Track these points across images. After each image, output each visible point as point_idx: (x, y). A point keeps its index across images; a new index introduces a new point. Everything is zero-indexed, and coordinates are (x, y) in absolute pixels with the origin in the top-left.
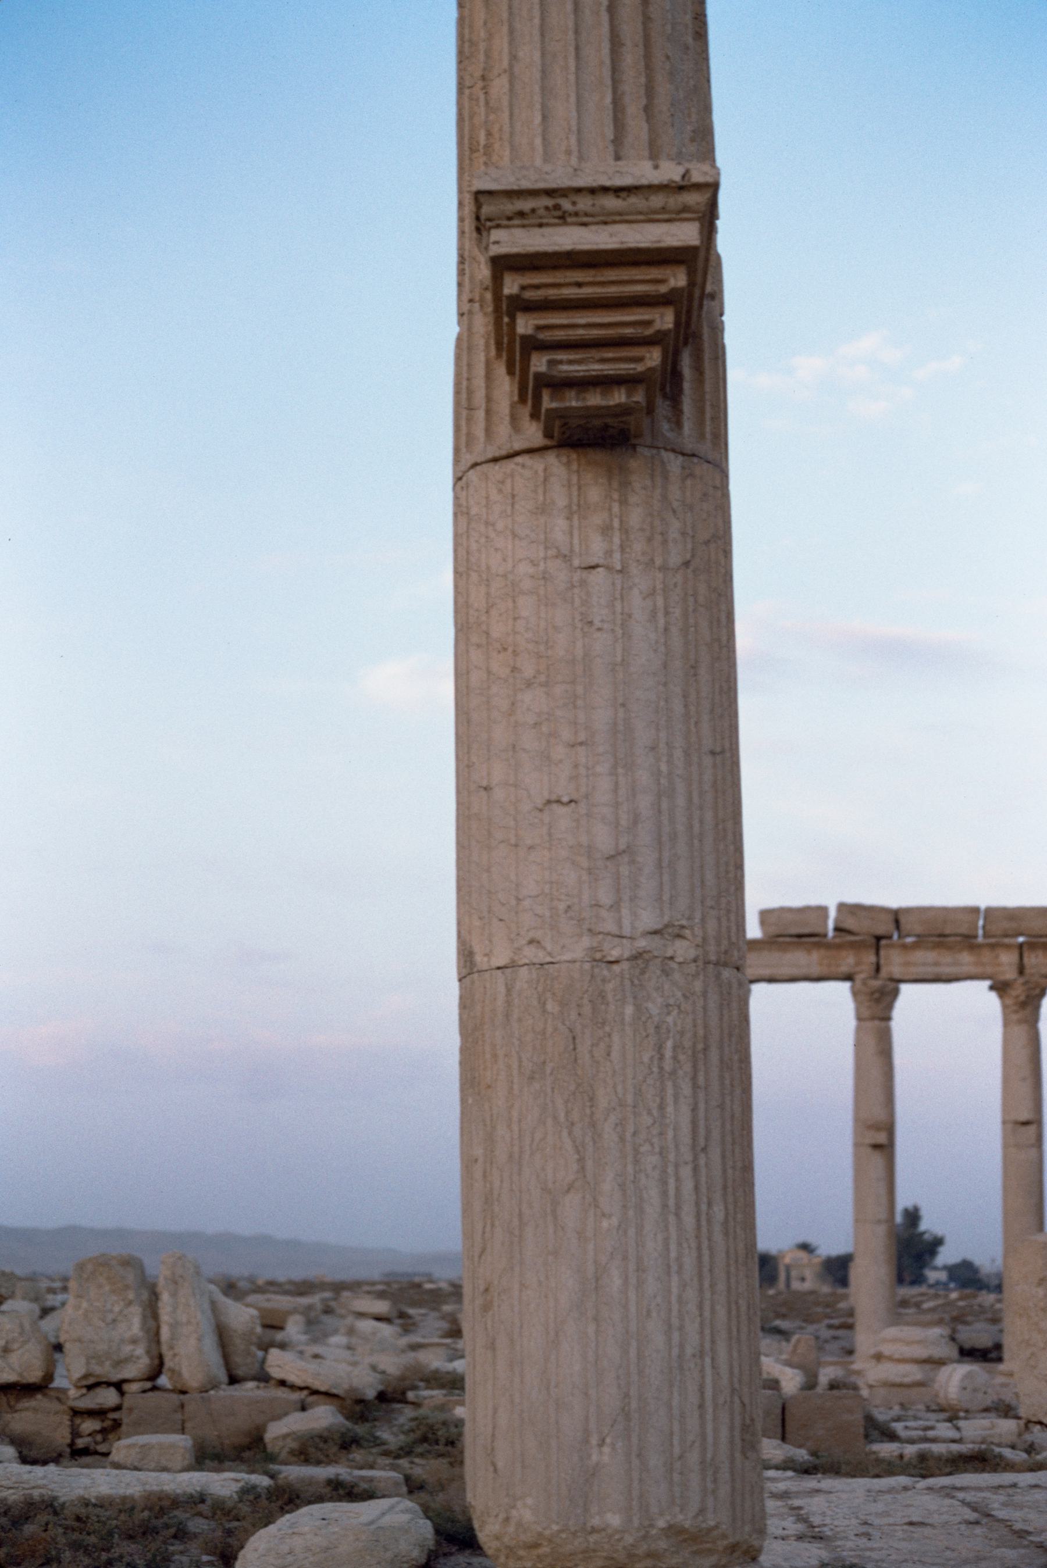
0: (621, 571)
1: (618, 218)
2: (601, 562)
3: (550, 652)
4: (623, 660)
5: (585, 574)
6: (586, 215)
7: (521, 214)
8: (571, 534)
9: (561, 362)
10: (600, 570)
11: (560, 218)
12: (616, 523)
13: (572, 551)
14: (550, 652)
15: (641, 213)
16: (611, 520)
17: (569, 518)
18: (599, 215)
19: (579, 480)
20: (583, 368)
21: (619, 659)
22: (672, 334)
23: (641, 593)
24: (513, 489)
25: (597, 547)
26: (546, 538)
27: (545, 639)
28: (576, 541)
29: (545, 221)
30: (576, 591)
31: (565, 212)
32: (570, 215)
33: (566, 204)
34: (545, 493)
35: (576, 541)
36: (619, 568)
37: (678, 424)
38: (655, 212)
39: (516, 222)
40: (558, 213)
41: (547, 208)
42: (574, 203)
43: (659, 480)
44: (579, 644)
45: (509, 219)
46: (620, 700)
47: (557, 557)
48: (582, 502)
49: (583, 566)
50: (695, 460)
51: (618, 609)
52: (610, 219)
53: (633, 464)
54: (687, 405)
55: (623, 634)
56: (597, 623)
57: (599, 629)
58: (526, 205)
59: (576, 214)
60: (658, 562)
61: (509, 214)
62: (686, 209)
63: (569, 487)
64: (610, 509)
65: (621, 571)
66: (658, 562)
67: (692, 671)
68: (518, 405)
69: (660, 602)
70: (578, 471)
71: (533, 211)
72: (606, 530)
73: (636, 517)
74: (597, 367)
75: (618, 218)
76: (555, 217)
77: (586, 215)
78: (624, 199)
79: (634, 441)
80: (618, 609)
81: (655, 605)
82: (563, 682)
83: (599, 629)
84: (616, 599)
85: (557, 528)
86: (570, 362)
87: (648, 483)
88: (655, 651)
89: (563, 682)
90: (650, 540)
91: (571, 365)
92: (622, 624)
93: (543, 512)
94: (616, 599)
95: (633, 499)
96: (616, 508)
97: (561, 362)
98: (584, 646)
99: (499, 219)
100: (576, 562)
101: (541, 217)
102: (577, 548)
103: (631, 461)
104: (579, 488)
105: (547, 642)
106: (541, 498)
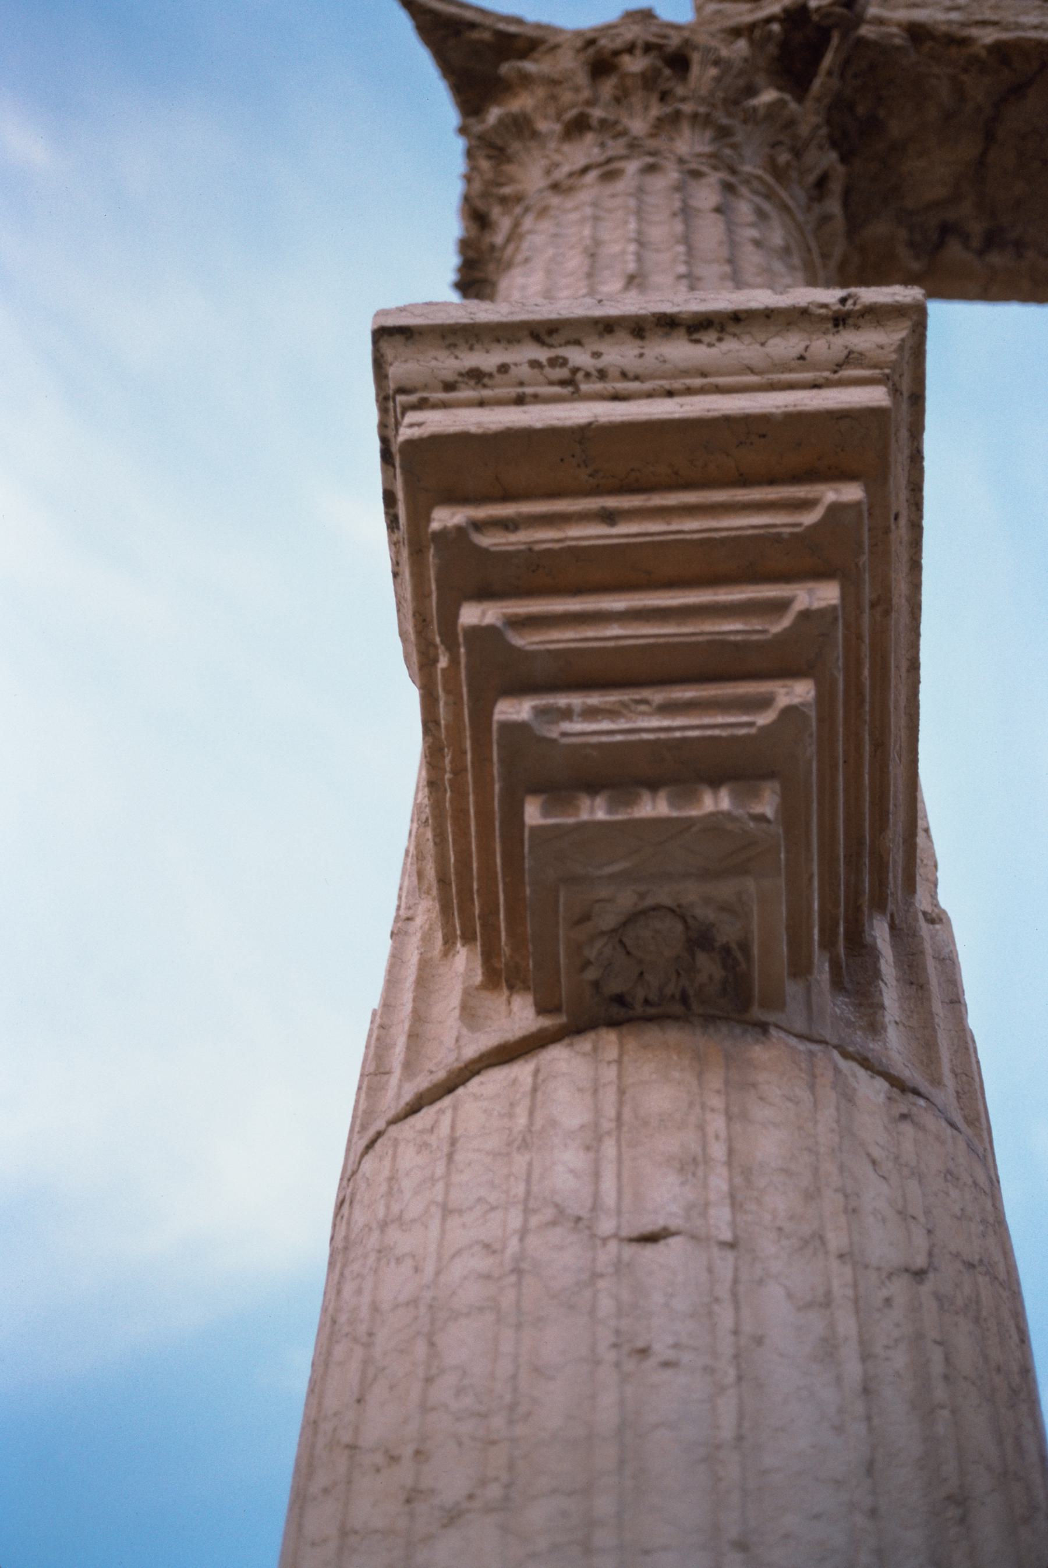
0: (732, 1245)
1: (698, 382)
2: (674, 1224)
3: (520, 1430)
4: (740, 1438)
5: (630, 1251)
6: (624, 375)
7: (476, 376)
8: (596, 1176)
9: (567, 714)
10: (673, 1241)
11: (563, 383)
12: (718, 1151)
13: (596, 1206)
14: (520, 1430)
15: (751, 370)
16: (704, 1146)
17: (593, 1148)
18: (652, 377)
19: (620, 1076)
20: (622, 724)
21: (727, 1433)
22: (840, 609)
23: (790, 1295)
24: (453, 1127)
25: (665, 1198)
26: (528, 1193)
27: (508, 1398)
28: (608, 1185)
29: (529, 390)
30: (602, 1284)
31: (575, 370)
32: (588, 375)
33: (578, 357)
34: (531, 1113)
35: (608, 1185)
36: (727, 1235)
37: (875, 1028)
38: (786, 368)
39: (465, 393)
40: (563, 373)
41: (535, 364)
42: (597, 355)
43: (830, 1097)
44: (608, 1399)
45: (449, 387)
46: (733, 1532)
47: (554, 1223)
48: (627, 1115)
49: (625, 1233)
50: (922, 1102)
51: (726, 1318)
52: (677, 384)
53: (759, 1052)
54: (890, 996)
55: (740, 1378)
56: (662, 1350)
57: (666, 1364)
58: (487, 359)
59: (603, 375)
60: (836, 1241)
61: (450, 377)
62: (851, 358)
63: (595, 1091)
64: (701, 1127)
65: (732, 1245)
66: (836, 1241)
67: (953, 1512)
68: (485, 994)
69: (847, 1325)
70: (619, 1062)
71: (504, 368)
72: (691, 1165)
73: (769, 1145)
74: (655, 722)
75: (698, 382)
76: (551, 383)
77: (624, 375)
78: (710, 345)
79: (757, 1013)
80: (726, 1318)
81: (832, 1325)
82: (554, 1491)
83: (666, 1364)
84: (717, 1300)
85: (560, 1168)
86: (591, 713)
87: (804, 1095)
88: (839, 1429)
89: (554, 1491)
90: (811, 1195)
91: (589, 722)
92: (736, 1356)
93: (525, 1145)
94: (722, 1389)
95: (761, 1113)
96: (717, 1123)
97: (567, 714)
98: (622, 1402)
99: (426, 387)
100: (606, 1226)
101: (521, 384)
102: (609, 1199)
103: (758, 1048)
104: (621, 1092)
105: (512, 1407)
106: (522, 1121)
